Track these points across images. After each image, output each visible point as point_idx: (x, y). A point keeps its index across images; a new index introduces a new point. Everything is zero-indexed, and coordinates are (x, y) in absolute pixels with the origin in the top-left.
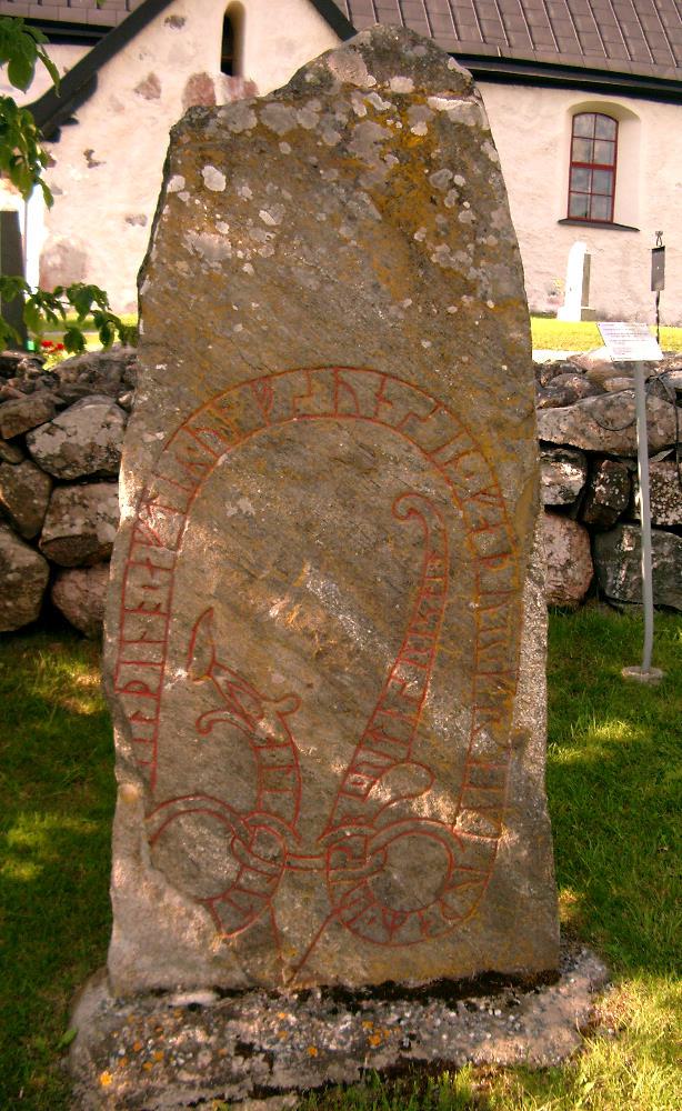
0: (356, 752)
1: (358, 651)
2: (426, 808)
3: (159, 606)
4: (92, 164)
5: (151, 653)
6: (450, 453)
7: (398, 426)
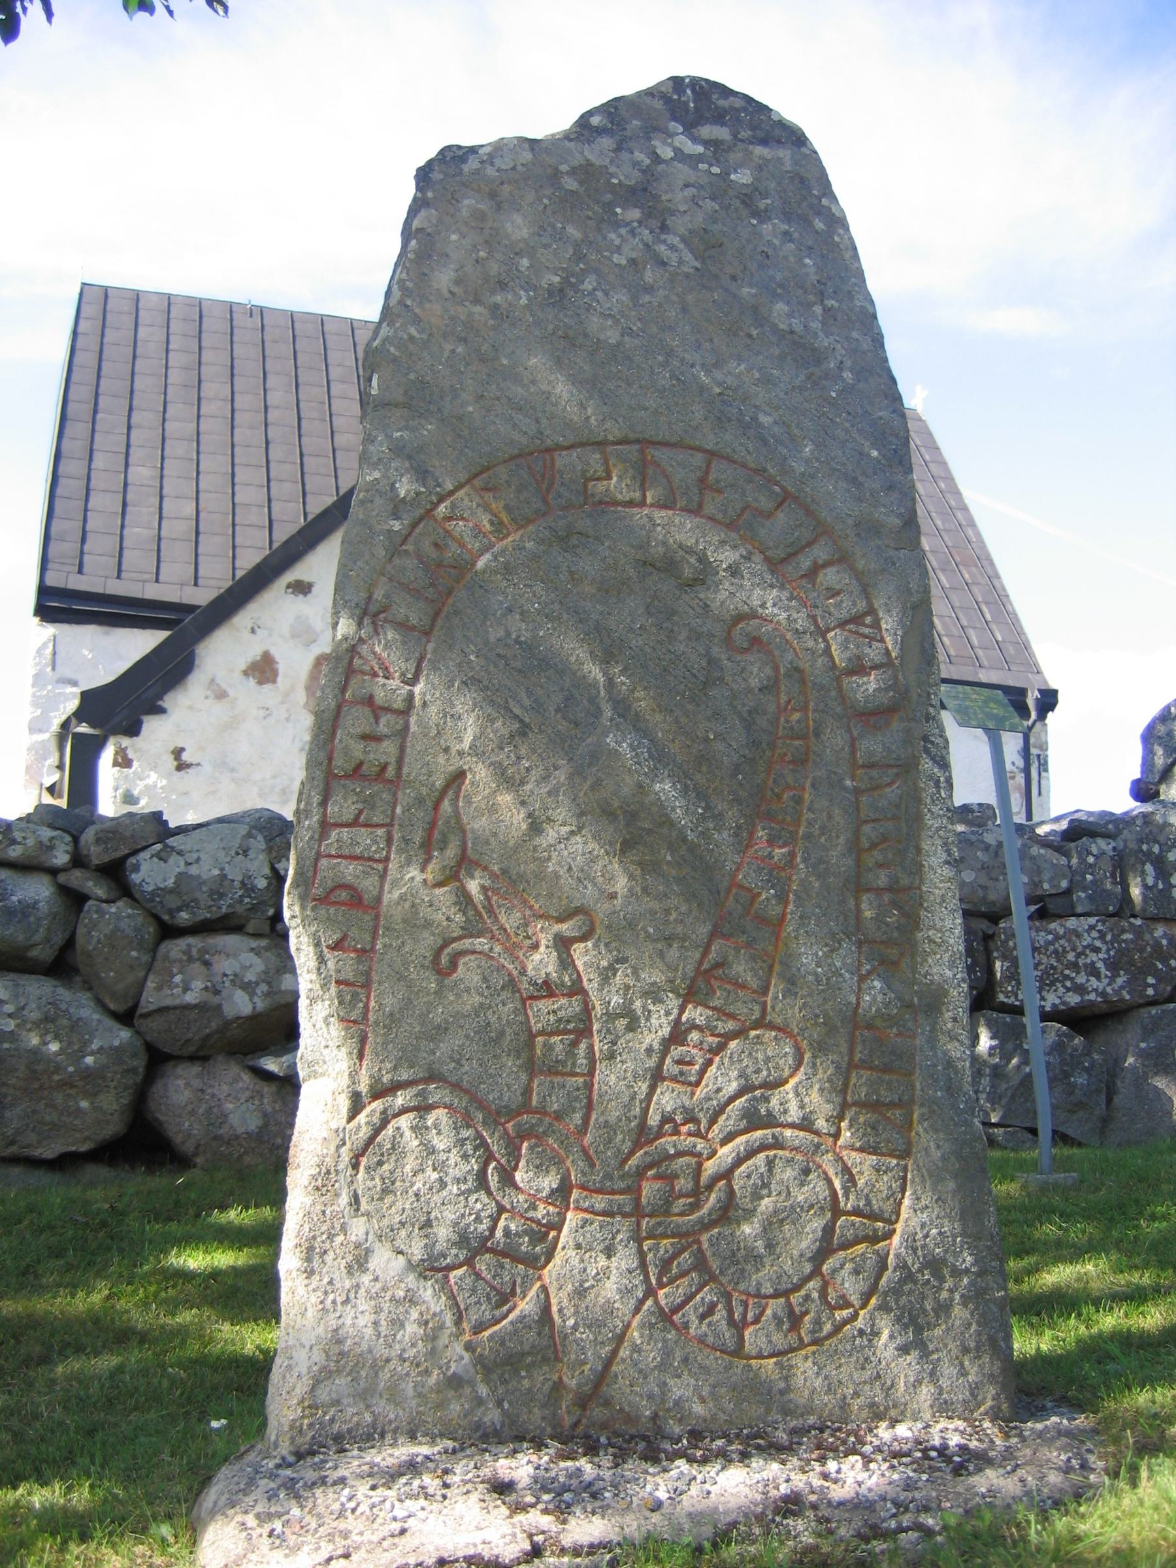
0: (682, 1010)
1: (684, 840)
2: (793, 1106)
3: (384, 768)
4: (182, 766)
5: (365, 840)
6: (805, 563)
7: (731, 523)
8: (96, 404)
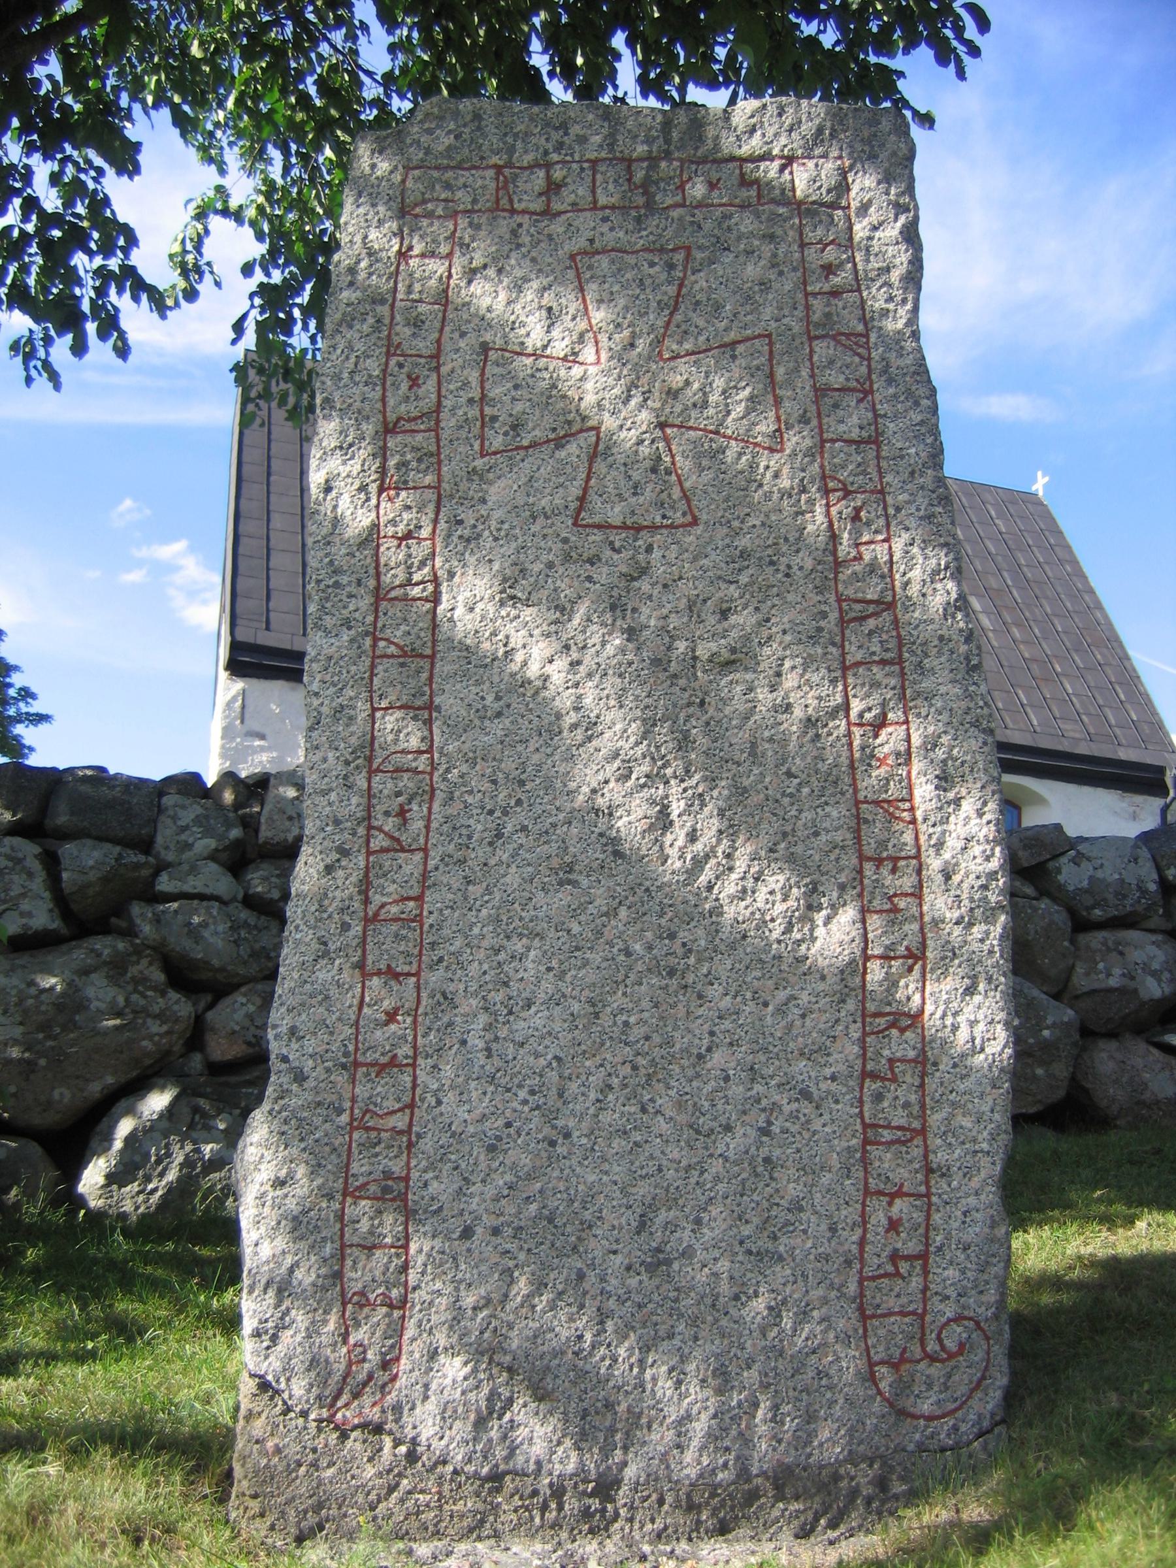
8: (269, 467)
